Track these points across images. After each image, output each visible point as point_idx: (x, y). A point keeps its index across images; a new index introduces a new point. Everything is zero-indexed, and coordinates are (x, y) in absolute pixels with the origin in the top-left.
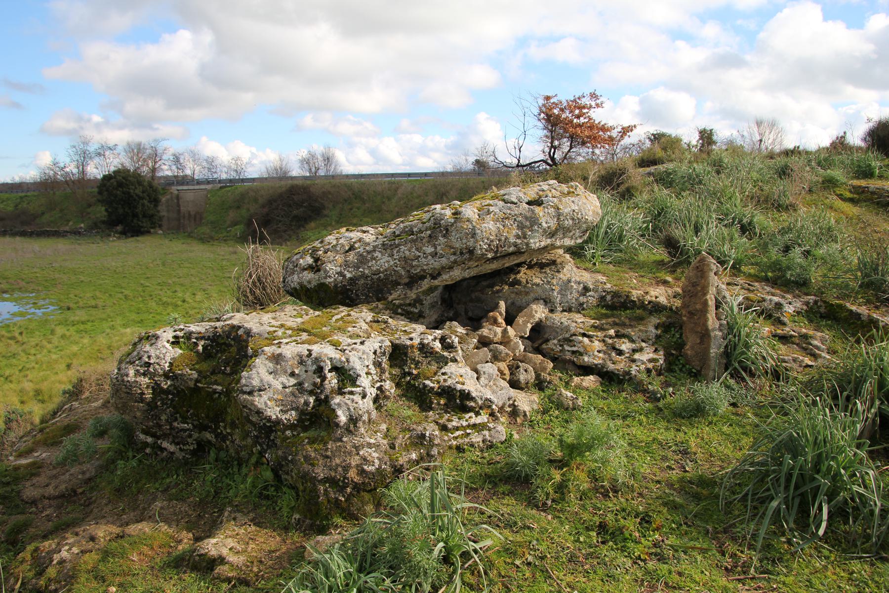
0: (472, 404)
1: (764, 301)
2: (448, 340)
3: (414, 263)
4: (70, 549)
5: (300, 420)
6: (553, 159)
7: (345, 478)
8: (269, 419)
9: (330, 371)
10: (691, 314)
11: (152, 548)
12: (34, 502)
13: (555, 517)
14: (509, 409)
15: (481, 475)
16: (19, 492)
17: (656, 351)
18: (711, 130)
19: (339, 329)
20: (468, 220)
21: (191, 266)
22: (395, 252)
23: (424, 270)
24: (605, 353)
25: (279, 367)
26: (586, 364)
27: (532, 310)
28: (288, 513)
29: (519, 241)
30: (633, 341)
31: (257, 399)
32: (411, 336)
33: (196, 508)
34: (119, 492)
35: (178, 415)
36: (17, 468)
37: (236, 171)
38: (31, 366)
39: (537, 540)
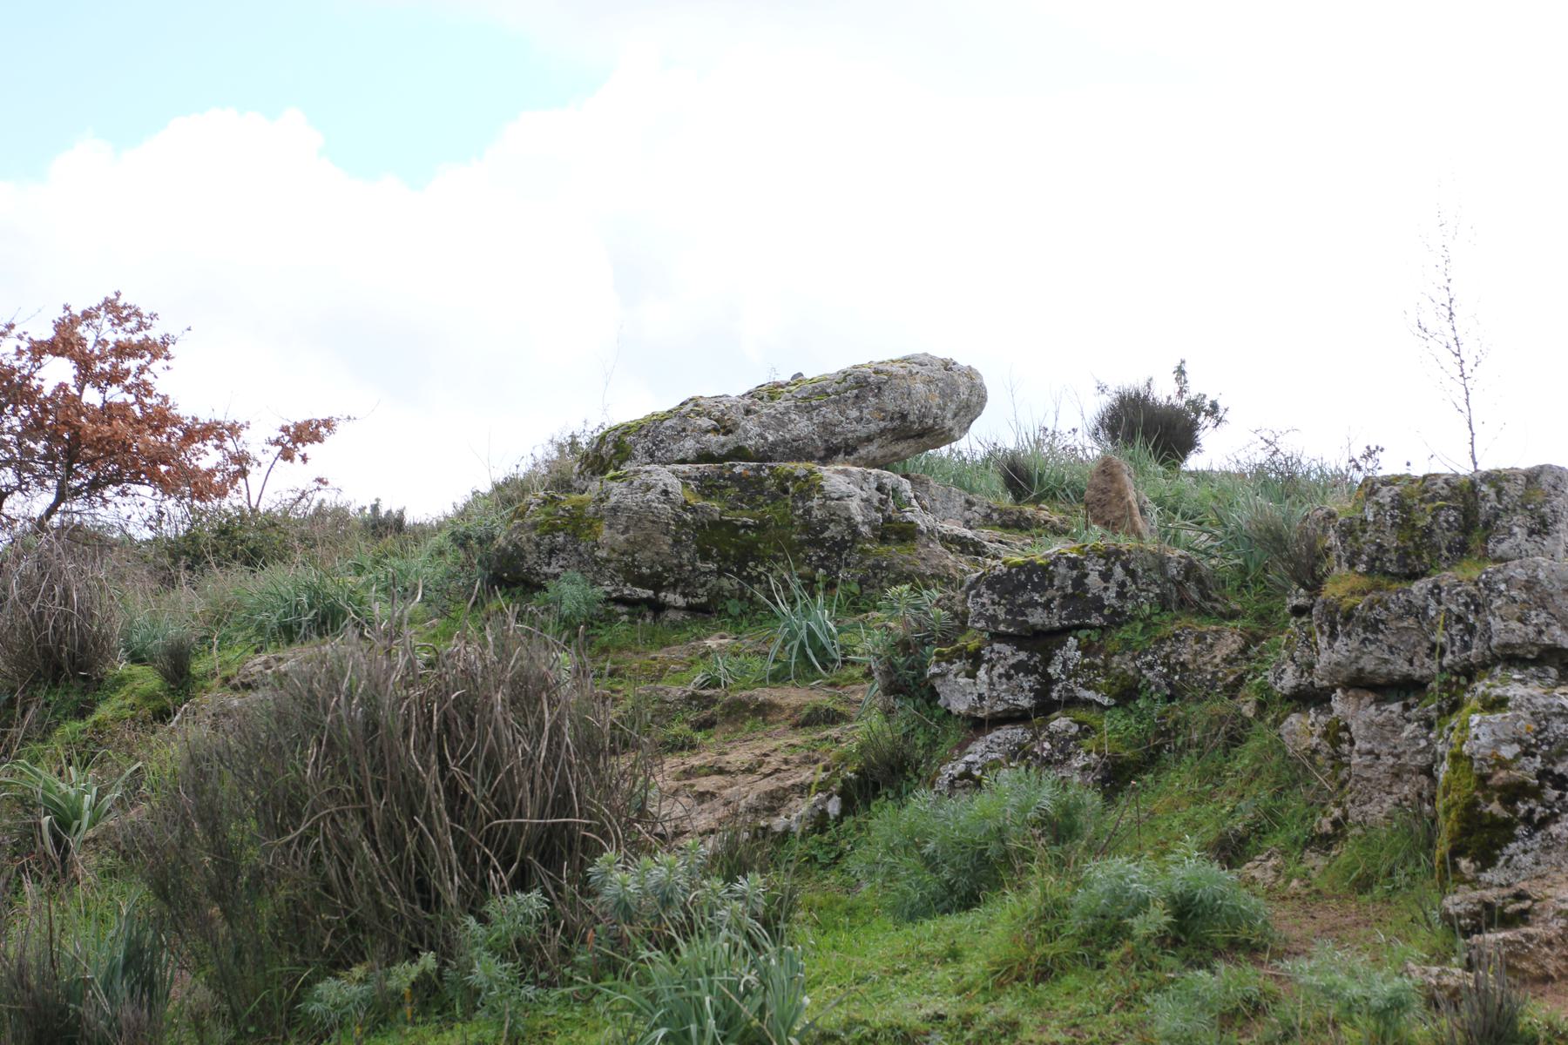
3: (838, 429)
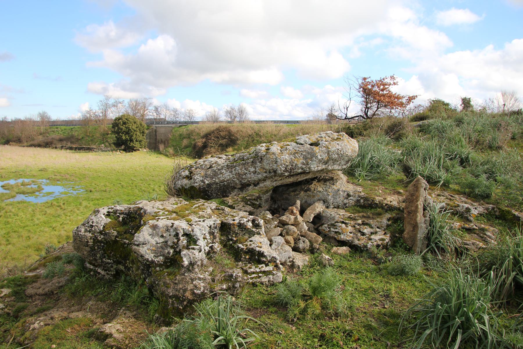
0: (264, 259)
1: (459, 206)
2: (256, 222)
4: (39, 323)
5: (165, 262)
6: (366, 114)
7: (184, 296)
8: (147, 260)
9: (182, 236)
10: (409, 213)
11: (80, 326)
12: (31, 297)
13: (297, 328)
14: (289, 264)
15: (261, 301)
16: (25, 290)
17: (385, 234)
18: (469, 99)
19: (194, 212)
20: (273, 154)
21: (160, 170)
22: (233, 170)
23: (249, 181)
24: (354, 234)
25: (155, 232)
26: (342, 240)
27: (315, 206)
28: (154, 313)
29: (304, 166)
30: (372, 228)
31: (141, 249)
32: (234, 218)
33: (110, 306)
34: (74, 294)
35: (106, 255)
36: (26, 278)
37: (189, 117)
38: (67, 222)
39: (282, 340)
